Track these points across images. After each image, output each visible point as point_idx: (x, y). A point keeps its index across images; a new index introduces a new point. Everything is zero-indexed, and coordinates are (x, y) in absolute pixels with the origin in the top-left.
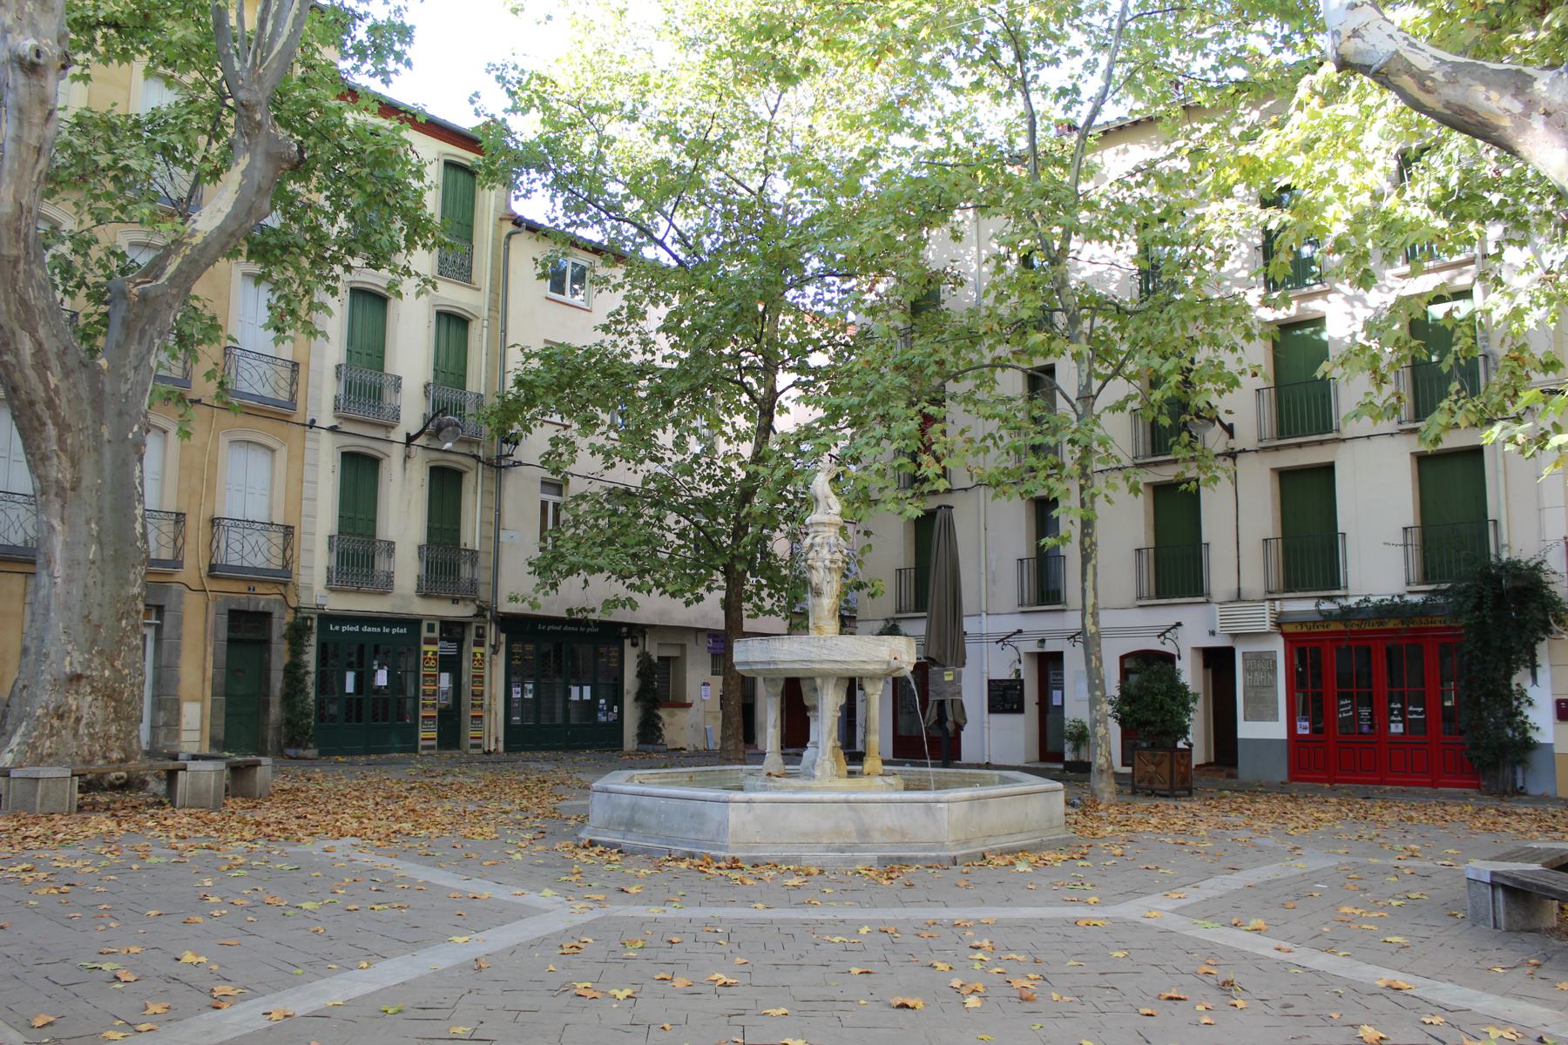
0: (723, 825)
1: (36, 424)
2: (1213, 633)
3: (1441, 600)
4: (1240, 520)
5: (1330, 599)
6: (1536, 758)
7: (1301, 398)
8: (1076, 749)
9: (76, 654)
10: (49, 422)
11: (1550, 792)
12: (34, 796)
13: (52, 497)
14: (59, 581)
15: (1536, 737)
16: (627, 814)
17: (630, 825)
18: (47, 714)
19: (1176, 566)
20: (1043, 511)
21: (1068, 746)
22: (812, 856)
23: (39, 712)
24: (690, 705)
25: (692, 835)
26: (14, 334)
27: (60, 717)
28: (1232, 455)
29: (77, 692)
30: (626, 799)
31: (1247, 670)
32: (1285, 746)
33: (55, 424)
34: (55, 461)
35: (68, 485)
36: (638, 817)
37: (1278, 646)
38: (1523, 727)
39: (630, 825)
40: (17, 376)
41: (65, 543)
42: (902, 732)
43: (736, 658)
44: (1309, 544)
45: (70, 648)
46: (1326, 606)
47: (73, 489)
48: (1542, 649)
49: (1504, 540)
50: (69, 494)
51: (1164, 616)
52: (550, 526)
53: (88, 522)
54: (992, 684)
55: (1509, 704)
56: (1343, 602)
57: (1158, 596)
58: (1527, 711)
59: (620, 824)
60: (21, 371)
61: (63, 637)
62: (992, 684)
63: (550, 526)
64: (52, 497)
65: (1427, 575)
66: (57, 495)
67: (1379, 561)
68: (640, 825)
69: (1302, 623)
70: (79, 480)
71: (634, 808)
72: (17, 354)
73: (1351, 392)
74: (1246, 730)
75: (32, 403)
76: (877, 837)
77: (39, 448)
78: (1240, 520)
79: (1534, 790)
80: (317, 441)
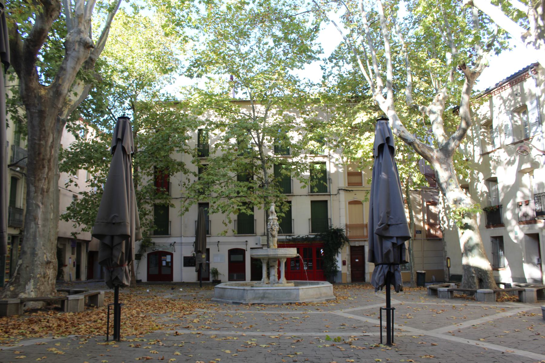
0: (298, 295)
1: (41, 167)
2: (257, 244)
3: (318, 237)
5: (290, 236)
6: (338, 273)
8: (214, 276)
9: (48, 254)
10: (46, 167)
11: (340, 282)
12: (77, 306)
13: (39, 194)
14: (40, 226)
15: (338, 269)
16: (262, 295)
17: (263, 298)
18: (41, 277)
20: (203, 206)
21: (211, 276)
22: (315, 301)
23: (38, 276)
24: (66, 266)
25: (287, 298)
26: (49, 134)
27: (44, 277)
29: (49, 268)
30: (261, 291)
33: (48, 168)
34: (43, 181)
35: (45, 190)
36: (266, 296)
38: (336, 267)
39: (263, 298)
40: (42, 150)
41: (43, 212)
42: (150, 273)
45: (45, 251)
46: (288, 237)
47: (47, 192)
48: (340, 250)
49: (333, 223)
50: (45, 193)
51: (243, 239)
53: (51, 205)
54: (185, 258)
55: (333, 262)
56: (294, 237)
57: (238, 234)
58: (337, 263)
60: (45, 148)
61: (43, 248)
62: (185, 258)
64: (39, 194)
65: (313, 231)
66: (41, 194)
67: (302, 227)
68: (267, 298)
70: (49, 189)
71: (264, 293)
72: (46, 142)
73: (297, 186)
75: (43, 159)
76: (323, 295)
77: (39, 176)
79: (337, 282)
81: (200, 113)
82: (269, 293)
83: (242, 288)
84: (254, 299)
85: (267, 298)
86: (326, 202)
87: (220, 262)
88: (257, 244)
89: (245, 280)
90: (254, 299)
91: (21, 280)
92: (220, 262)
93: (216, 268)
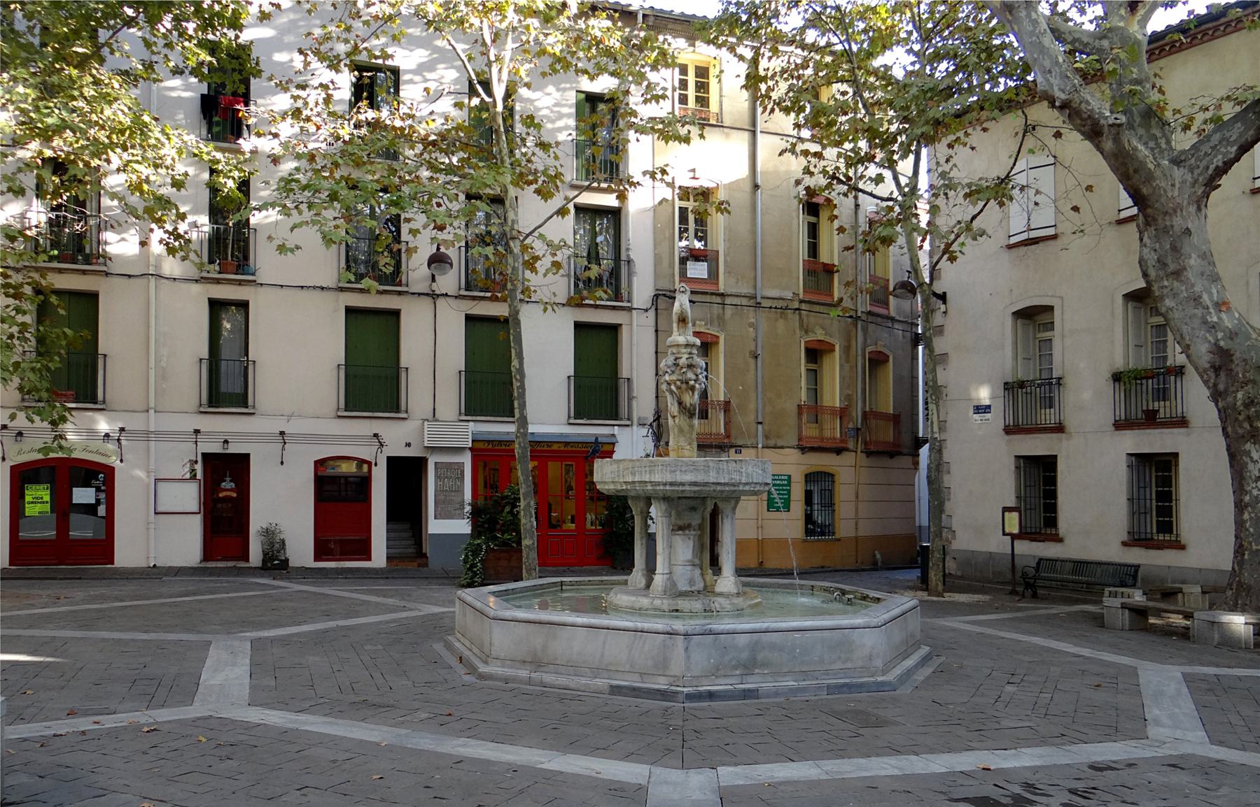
2: (408, 445)
4: (433, 345)
7: (600, 273)
16: (745, 655)
17: (749, 667)
19: (372, 379)
25: (839, 665)
28: (434, 296)
30: (743, 640)
31: (437, 477)
32: (71, 527)
36: (760, 657)
37: (466, 460)
39: (749, 667)
43: (597, 477)
44: (491, 378)
51: (364, 427)
52: (489, 294)
59: (736, 668)
63: (489, 294)
68: (764, 665)
69: (489, 442)
71: (754, 648)
74: (435, 526)
78: (433, 345)
80: (657, 276)
81: (173, 20)
82: (773, 647)
83: (659, 625)
84: (715, 672)
85: (764, 665)
86: (614, 329)
87: (282, 506)
88: (408, 445)
89: (369, 559)
90: (715, 672)
91: (323, 264)
92: (282, 506)
93: (274, 522)
